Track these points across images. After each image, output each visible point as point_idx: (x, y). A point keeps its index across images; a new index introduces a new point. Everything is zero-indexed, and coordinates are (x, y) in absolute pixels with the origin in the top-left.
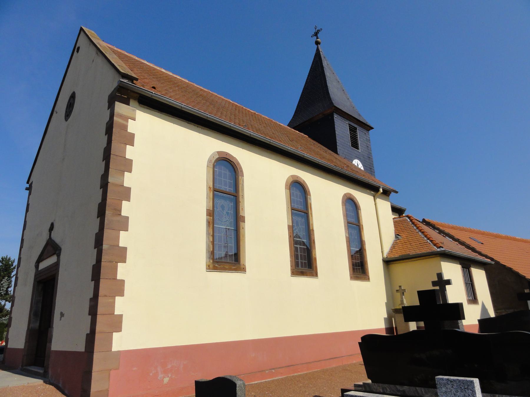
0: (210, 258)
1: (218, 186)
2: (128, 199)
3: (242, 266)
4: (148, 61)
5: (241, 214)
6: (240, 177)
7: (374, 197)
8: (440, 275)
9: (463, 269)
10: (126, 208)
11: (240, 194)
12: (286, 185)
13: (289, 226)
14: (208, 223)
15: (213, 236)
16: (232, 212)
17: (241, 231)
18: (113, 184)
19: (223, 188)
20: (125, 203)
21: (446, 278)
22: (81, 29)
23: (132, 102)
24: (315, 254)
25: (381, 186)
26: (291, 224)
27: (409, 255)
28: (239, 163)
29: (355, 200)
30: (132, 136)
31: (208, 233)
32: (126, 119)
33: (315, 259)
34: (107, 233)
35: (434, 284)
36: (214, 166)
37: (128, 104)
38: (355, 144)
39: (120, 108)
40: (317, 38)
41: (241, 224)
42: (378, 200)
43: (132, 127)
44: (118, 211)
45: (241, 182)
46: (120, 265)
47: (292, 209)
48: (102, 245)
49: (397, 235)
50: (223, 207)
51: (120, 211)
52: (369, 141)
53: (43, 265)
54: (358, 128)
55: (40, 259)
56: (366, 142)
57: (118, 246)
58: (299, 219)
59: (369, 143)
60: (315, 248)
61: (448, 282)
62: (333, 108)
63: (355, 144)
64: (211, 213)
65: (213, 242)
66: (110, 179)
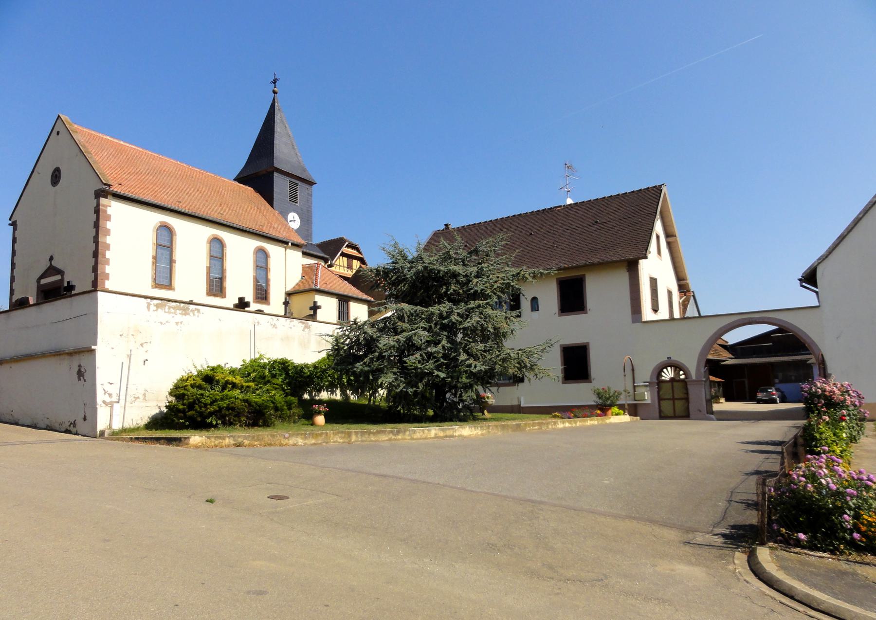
0: (153, 282)
1: (160, 242)
2: (109, 250)
3: (173, 288)
4: (110, 136)
5: (174, 258)
6: (174, 237)
7: (285, 248)
8: (315, 303)
9: (339, 303)
10: (108, 254)
11: (174, 246)
12: (208, 241)
13: (207, 267)
14: (153, 263)
15: (156, 270)
16: (168, 257)
17: (173, 268)
18: (102, 242)
19: (163, 243)
20: (107, 252)
21: (318, 304)
22: (59, 116)
23: (109, 196)
24: (225, 285)
25: (290, 242)
26: (209, 265)
27: (298, 290)
28: (173, 228)
29: (266, 250)
30: (110, 216)
31: (153, 269)
32: (106, 206)
33: (225, 288)
34: (100, 266)
35: (311, 308)
36: (157, 230)
37: (107, 198)
38: (294, 198)
39: (103, 201)
40: (275, 87)
41: (174, 264)
42: (288, 251)
43: (109, 211)
44: (104, 256)
45: (174, 239)
46: (106, 281)
47: (211, 256)
48: (98, 271)
49: (303, 276)
50: (162, 254)
51: (105, 255)
52: (311, 195)
53: (43, 281)
54: (300, 183)
55: (43, 276)
56: (307, 196)
57: (105, 272)
58: (216, 263)
59: (310, 197)
60: (226, 281)
61: (319, 307)
62: (274, 168)
63: (294, 198)
64: (154, 258)
65: (155, 273)
66: (100, 240)
